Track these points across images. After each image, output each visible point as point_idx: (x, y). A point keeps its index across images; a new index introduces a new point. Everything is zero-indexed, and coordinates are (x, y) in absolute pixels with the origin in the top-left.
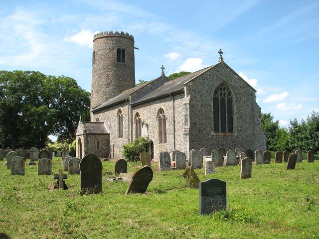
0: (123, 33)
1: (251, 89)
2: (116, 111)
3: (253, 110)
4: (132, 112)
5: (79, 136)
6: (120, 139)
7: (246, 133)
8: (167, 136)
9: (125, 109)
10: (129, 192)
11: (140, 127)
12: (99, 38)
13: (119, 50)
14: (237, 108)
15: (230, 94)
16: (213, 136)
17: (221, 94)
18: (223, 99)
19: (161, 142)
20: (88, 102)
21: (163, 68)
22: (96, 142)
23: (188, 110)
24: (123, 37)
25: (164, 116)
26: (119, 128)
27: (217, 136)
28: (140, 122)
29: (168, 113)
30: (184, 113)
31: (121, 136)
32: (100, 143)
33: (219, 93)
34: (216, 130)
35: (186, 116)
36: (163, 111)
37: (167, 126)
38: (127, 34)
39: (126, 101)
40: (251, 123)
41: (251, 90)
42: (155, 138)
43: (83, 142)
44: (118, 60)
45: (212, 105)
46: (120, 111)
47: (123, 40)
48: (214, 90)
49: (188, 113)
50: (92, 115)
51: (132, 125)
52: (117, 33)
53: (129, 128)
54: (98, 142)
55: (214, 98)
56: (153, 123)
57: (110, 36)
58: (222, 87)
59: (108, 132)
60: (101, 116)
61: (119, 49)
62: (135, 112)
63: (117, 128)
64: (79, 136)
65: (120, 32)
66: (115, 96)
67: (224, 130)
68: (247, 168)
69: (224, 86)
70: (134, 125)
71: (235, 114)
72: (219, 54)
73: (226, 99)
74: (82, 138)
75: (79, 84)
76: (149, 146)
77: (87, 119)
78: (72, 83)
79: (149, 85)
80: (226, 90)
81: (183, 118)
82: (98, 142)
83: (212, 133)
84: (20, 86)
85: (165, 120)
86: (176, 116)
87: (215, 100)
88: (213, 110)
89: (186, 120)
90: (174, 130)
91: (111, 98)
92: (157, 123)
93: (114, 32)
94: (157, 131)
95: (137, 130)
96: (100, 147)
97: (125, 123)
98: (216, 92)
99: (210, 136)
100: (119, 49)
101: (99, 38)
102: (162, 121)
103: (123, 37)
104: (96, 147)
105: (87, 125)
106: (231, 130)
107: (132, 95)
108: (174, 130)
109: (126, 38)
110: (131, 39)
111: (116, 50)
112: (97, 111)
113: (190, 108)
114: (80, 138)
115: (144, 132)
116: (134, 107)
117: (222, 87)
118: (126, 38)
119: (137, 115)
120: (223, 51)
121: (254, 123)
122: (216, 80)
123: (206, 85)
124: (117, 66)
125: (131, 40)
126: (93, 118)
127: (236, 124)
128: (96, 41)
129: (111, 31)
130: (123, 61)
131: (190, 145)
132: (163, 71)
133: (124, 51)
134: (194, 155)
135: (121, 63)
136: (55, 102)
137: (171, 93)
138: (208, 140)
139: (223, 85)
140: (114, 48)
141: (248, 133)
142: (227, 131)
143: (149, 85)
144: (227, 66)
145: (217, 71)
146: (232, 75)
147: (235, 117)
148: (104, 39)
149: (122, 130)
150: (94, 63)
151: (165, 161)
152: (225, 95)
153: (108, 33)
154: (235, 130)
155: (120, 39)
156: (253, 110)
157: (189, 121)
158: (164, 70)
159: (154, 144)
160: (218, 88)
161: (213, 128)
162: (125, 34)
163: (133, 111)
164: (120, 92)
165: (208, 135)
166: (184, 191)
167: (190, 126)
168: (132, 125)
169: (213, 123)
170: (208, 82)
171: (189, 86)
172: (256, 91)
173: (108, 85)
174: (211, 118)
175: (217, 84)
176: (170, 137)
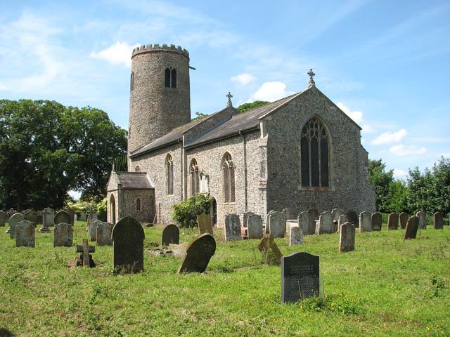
0: (173, 47)
1: (354, 126)
2: (163, 156)
3: (356, 155)
4: (186, 158)
5: (111, 191)
6: (169, 196)
7: (347, 187)
8: (236, 191)
9: (177, 154)
10: (182, 270)
11: (198, 179)
12: (139, 54)
13: (167, 71)
14: (334, 153)
15: (324, 132)
16: (301, 191)
17: (312, 133)
18: (314, 140)
19: (227, 200)
20: (124, 144)
21: (230, 96)
22: (135, 200)
23: (266, 155)
24: (173, 53)
25: (231, 164)
26: (169, 180)
27: (306, 191)
28: (197, 172)
29: (237, 160)
30: (259, 160)
31: (170, 191)
32: (141, 202)
33: (308, 132)
34: (305, 183)
35: (262, 163)
36: (230, 156)
37: (236, 177)
38: (180, 48)
39: (178, 143)
40: (354, 173)
41: (354, 127)
42: (218, 195)
43: (116, 200)
44: (167, 84)
45: (300, 148)
46: (169, 157)
47: (174, 56)
48: (301, 127)
49: (266, 159)
50: (130, 162)
51: (186, 176)
52: (165, 46)
53: (182, 181)
54: (138, 200)
55: (302, 138)
56: (216, 173)
57: (155, 51)
58: (314, 122)
59: (153, 186)
60: (142, 164)
61: (168, 69)
62: (190, 158)
63: (165, 180)
64: (111, 191)
65: (169, 46)
66: (162, 135)
67: (315, 184)
68: (349, 236)
69: (316, 121)
70: (189, 177)
71: (331, 161)
72: (309, 77)
73: (319, 139)
74: (116, 195)
75: (112, 118)
76: (210, 205)
77: (122, 168)
78: (101, 117)
79: (211, 121)
80: (319, 127)
81: (258, 166)
82: (138, 200)
83: (300, 188)
84: (29, 121)
85: (232, 169)
86: (248, 163)
87: (304, 141)
88: (300, 154)
89: (263, 170)
90: (246, 184)
91: (157, 138)
92: (221, 173)
93: (161, 46)
94: (221, 185)
95: (193, 184)
96: (141, 207)
97: (177, 173)
98: (304, 130)
99: (296, 192)
100: (168, 69)
101: (139, 54)
102: (229, 171)
103: (173, 53)
104: (136, 207)
105: (123, 176)
106: (326, 184)
107: (186, 134)
108: (246, 184)
109: (178, 53)
110: (184, 55)
111: (163, 70)
112: (137, 157)
113: (268, 152)
114: (112, 195)
115: (204, 187)
116: (189, 150)
117: (314, 122)
118: (178, 53)
119: (194, 162)
120: (314, 71)
121: (358, 173)
122: (305, 113)
123: (290, 120)
124: (165, 93)
125: (185, 56)
126: (131, 166)
127: (332, 175)
128: (135, 58)
129: (157, 43)
130: (174, 86)
131: (268, 205)
132: (229, 100)
133: (174, 72)
134: (274, 218)
135: (170, 89)
136: (78, 144)
137: (241, 132)
138: (293, 197)
139: (314, 119)
140: (160, 67)
141: (350, 187)
142: (320, 185)
143: (211, 121)
144: (321, 94)
145: (306, 100)
146: (327, 105)
147: (331, 165)
148: (146, 55)
149: (172, 183)
150: (132, 88)
151: (233, 227)
152: (317, 133)
153: (153, 46)
154: (331, 183)
155: (170, 54)
156: (356, 155)
157: (266, 171)
158: (231, 99)
159: (217, 203)
160: (307, 124)
161: (300, 181)
162: (176, 47)
163: (188, 156)
164: (170, 129)
165: (294, 190)
166: (260, 270)
167: (268, 178)
168: (186, 176)
169: (300, 173)
170: (293, 116)
171: (267, 121)
172: (361, 129)
173: (152, 120)
174: (297, 167)
175: (306, 119)
176: (239, 193)
